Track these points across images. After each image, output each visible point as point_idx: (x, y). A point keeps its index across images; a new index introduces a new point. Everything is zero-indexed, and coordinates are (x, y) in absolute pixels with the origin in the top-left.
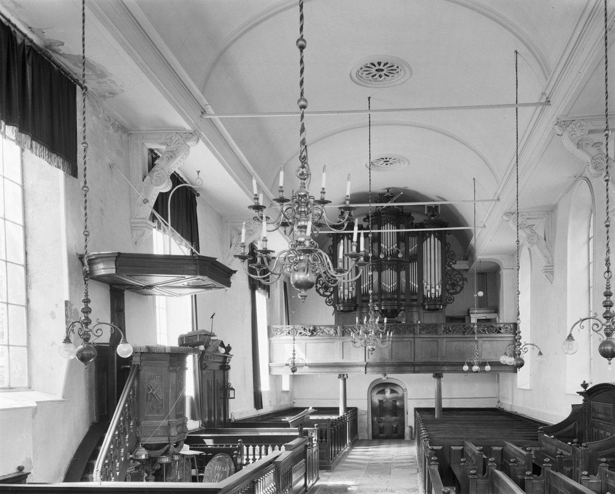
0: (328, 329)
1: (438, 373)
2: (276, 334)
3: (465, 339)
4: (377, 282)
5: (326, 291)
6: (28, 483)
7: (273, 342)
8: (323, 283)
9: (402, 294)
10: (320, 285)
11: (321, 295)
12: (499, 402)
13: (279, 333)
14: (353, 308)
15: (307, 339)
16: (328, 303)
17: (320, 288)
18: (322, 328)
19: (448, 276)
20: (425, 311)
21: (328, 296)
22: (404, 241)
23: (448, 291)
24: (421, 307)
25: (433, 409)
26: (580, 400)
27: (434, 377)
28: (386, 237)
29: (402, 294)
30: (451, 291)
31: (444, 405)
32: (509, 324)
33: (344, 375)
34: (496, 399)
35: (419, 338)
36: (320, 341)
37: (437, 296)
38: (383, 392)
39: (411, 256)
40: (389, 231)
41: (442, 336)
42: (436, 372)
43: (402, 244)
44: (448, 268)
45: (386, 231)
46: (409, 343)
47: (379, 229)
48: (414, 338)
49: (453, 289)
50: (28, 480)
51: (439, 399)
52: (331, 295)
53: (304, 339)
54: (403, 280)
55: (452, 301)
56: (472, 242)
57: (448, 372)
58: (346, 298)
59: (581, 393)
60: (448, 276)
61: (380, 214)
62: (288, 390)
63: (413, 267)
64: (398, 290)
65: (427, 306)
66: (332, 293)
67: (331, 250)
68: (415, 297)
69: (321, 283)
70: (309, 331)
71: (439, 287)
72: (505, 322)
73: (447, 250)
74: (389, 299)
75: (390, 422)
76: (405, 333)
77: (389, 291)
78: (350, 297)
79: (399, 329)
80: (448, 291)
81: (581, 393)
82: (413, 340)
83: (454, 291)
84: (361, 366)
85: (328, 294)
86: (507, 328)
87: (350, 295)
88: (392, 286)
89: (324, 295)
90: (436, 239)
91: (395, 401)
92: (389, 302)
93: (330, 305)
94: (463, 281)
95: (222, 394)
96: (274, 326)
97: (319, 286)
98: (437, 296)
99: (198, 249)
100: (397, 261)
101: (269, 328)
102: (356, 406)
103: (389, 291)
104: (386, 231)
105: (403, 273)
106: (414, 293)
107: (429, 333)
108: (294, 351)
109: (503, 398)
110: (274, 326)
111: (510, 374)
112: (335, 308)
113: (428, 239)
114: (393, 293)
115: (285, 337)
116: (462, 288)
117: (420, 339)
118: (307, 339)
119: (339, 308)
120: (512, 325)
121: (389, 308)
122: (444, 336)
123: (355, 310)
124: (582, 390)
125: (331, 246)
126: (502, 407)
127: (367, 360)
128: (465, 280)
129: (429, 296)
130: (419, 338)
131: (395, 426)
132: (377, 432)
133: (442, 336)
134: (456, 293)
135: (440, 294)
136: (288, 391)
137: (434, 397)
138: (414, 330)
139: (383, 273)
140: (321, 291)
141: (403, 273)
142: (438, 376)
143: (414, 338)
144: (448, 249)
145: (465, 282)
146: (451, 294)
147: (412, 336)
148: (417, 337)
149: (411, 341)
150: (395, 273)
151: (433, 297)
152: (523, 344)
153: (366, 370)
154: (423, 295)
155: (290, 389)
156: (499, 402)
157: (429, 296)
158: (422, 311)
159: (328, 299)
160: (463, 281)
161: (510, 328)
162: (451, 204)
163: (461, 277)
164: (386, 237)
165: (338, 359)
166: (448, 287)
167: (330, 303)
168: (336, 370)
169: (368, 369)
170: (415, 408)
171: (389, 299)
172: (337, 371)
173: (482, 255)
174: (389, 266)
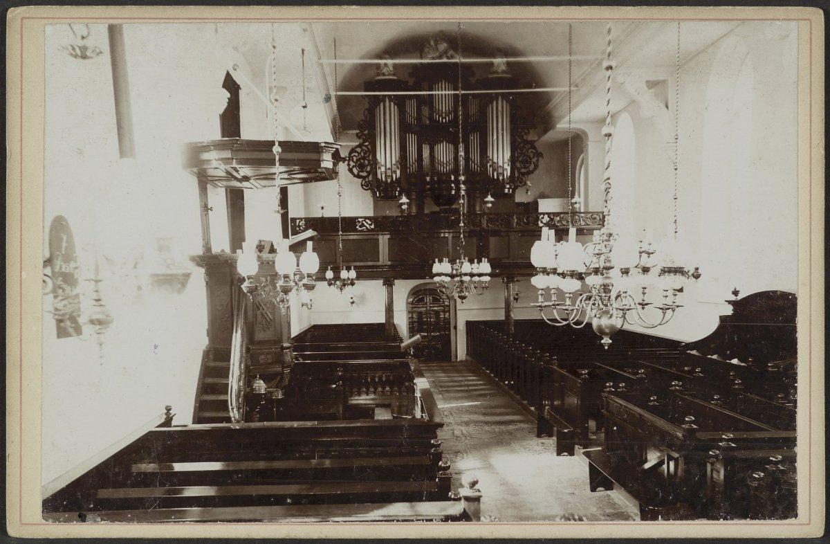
6: (174, 426)
8: (358, 160)
10: (354, 162)
11: (355, 176)
17: (353, 166)
18: (360, 220)
26: (729, 310)
28: (444, 102)
30: (523, 170)
37: (394, 179)
40: (444, 92)
45: (440, 93)
47: (431, 90)
49: (525, 168)
50: (174, 423)
52: (368, 176)
56: (551, 105)
59: (729, 302)
63: (474, 139)
69: (355, 160)
80: (519, 169)
81: (729, 302)
85: (364, 174)
86: (595, 218)
87: (394, 176)
89: (358, 176)
90: (392, 103)
97: (352, 164)
104: (440, 93)
116: (536, 167)
124: (733, 298)
125: (367, 109)
128: (539, 155)
135: (509, 174)
139: (436, 147)
140: (355, 171)
145: (540, 159)
146: (523, 174)
150: (451, 147)
151: (501, 178)
157: (384, 180)
159: (364, 182)
161: (598, 218)
164: (444, 102)
173: (576, 123)
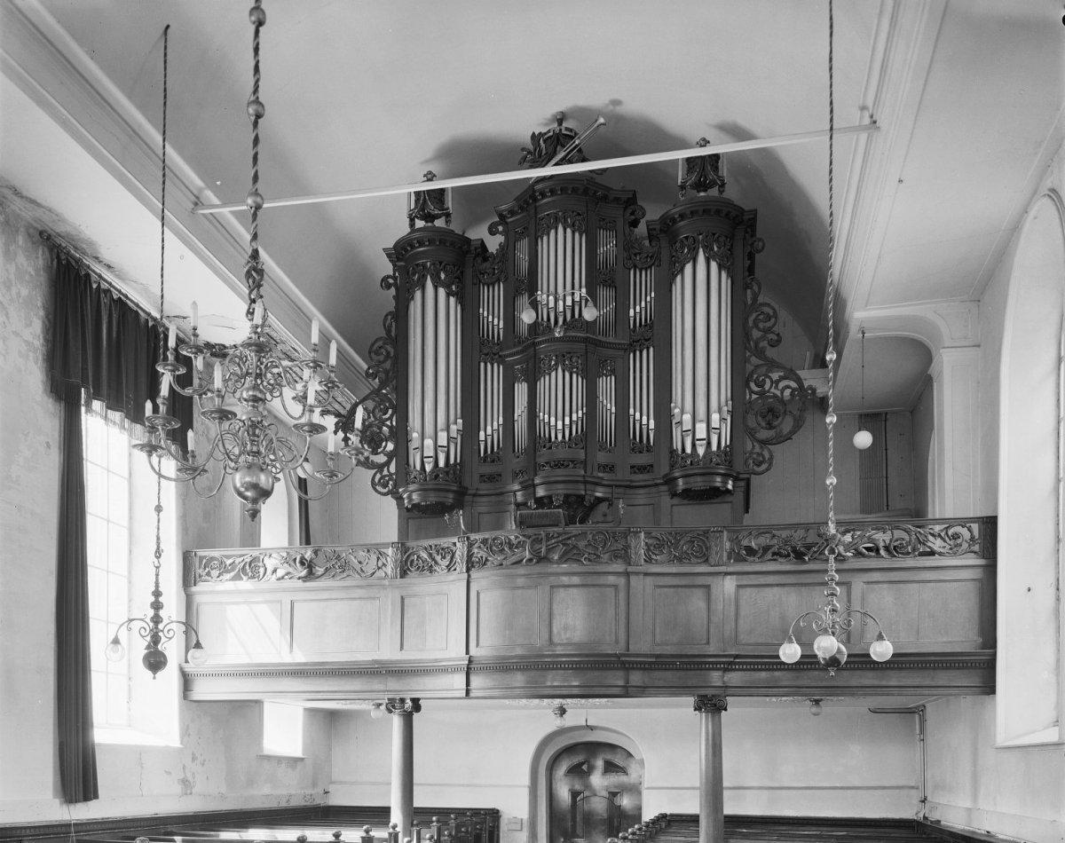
0: (362, 554)
1: (710, 692)
2: (208, 574)
5: (375, 452)
7: (198, 599)
9: (602, 448)
12: (924, 801)
13: (215, 573)
14: (451, 496)
15: (295, 590)
19: (752, 385)
20: (676, 501)
21: (380, 467)
22: (610, 283)
23: (751, 433)
24: (664, 488)
25: (694, 819)
27: (698, 708)
29: (602, 448)
30: (764, 434)
31: (729, 809)
32: (963, 522)
33: (402, 701)
34: (914, 791)
35: (646, 574)
36: (335, 595)
38: (579, 771)
41: (723, 569)
42: (703, 692)
43: (604, 293)
44: (754, 360)
46: (610, 592)
48: (627, 574)
49: (770, 426)
51: (714, 788)
52: (387, 464)
53: (284, 590)
54: (608, 404)
55: (764, 466)
57: (746, 690)
58: (428, 468)
60: (752, 385)
61: (535, 200)
62: (298, 753)
64: (587, 435)
65: (680, 482)
66: (390, 456)
67: (391, 325)
68: (641, 459)
70: (302, 563)
71: (722, 419)
72: (949, 515)
73: (750, 302)
74: (559, 464)
76: (596, 558)
78: (442, 464)
79: (575, 547)
82: (622, 581)
83: (771, 433)
84: (455, 670)
86: (956, 536)
88: (567, 421)
92: (559, 471)
96: (201, 553)
98: (714, 448)
99: (306, 493)
100: (586, 340)
101: (187, 559)
105: (606, 385)
106: (640, 447)
107: (680, 560)
108: (157, 594)
109: (936, 787)
110: (201, 553)
111: (966, 702)
112: (399, 499)
114: (572, 442)
115: (230, 585)
117: (649, 580)
118: (295, 590)
119: (410, 497)
120: (975, 527)
121: (561, 490)
122: (731, 569)
123: (459, 504)
126: (934, 816)
127: (473, 651)
129: (689, 450)
130: (646, 574)
133: (723, 569)
134: (782, 439)
136: (302, 759)
137: (698, 785)
138: (627, 548)
139: (540, 385)
141: (606, 385)
142: (712, 705)
143: (627, 574)
144: (755, 299)
146: (764, 443)
147: (618, 567)
148: (637, 574)
149: (616, 587)
152: (165, 621)
153: (468, 684)
154: (672, 452)
155: (305, 750)
156: (924, 801)
158: (666, 500)
159: (378, 476)
162: (764, 150)
163: (793, 384)
165: (388, 652)
166: (752, 422)
167: (385, 486)
168: (377, 685)
169: (476, 681)
171: (559, 464)
172: (381, 687)
174: (561, 358)
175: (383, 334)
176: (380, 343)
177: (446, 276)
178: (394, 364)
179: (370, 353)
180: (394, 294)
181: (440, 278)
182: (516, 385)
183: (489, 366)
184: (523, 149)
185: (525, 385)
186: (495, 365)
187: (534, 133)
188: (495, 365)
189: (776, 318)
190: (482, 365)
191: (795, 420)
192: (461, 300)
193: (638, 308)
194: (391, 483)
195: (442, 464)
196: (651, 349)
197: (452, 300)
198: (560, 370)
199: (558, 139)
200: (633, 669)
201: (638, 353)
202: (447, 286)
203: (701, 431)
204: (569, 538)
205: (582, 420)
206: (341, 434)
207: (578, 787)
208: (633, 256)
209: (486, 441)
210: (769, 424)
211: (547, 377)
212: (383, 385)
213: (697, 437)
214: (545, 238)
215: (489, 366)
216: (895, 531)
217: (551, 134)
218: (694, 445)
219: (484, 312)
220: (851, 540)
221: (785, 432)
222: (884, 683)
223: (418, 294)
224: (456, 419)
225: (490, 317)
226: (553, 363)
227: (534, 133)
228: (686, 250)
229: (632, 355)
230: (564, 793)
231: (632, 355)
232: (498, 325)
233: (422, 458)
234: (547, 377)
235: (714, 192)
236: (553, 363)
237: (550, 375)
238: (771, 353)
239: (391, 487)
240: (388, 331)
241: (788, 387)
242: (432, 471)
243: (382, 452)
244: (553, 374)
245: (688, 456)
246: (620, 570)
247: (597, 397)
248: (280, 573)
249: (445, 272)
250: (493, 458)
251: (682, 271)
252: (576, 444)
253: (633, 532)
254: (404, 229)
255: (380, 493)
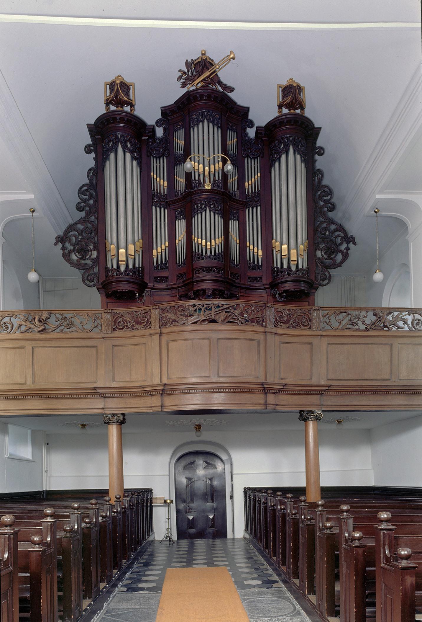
3: (368, 340)
4: (184, 241)
10: (72, 245)
16: (87, 282)
39: (248, 195)
55: (326, 282)
75: (204, 511)
77: (209, 253)
82: (261, 337)
91: (211, 479)
93: (91, 286)
94: (348, 243)
95: (44, 503)
102: (302, 85)
103: (209, 253)
105: (234, 225)
113: (284, 157)
116: (346, 256)
117: (277, 337)
131: (211, 517)
132: (185, 525)
139: (195, 221)
141: (234, 225)
147: (261, 329)
160: (348, 243)
163: (342, 235)
170: (245, 489)
175: (87, 181)
176: (86, 188)
177: (131, 146)
178: (96, 201)
179: (78, 194)
180: (94, 157)
181: (127, 146)
182: (177, 221)
183: (158, 209)
184: (180, 71)
185: (184, 222)
186: (162, 209)
187: (187, 61)
188: (162, 209)
189: (331, 195)
190: (154, 208)
191: (343, 256)
192: (140, 165)
193: (253, 179)
194: (95, 279)
195: (131, 266)
196: (259, 208)
197: (135, 163)
198: (208, 210)
199: (205, 64)
200: (270, 393)
201: (251, 209)
202: (132, 152)
203: (293, 257)
204: (228, 308)
205: (222, 244)
206: (60, 245)
207: (190, 475)
208: (247, 149)
209: (157, 256)
210: (329, 257)
211: (199, 215)
212: (88, 214)
213: (291, 259)
214: (196, 128)
215: (158, 209)
216: (415, 315)
217: (200, 60)
218: (289, 263)
219: (154, 175)
220: (392, 319)
221: (338, 262)
222: (411, 403)
223: (112, 156)
224: (139, 240)
225: (158, 179)
226: (203, 206)
227: (187, 61)
228: (282, 146)
229: (247, 210)
230: (183, 480)
231: (247, 210)
232: (164, 184)
233: (118, 261)
234: (199, 215)
235: (298, 111)
236: (203, 206)
237: (201, 213)
238: (330, 214)
239: (95, 282)
240: (91, 180)
241: (339, 236)
242: (125, 271)
243: (88, 259)
244: (204, 213)
245: (286, 270)
246: (262, 330)
247: (229, 232)
248: (23, 328)
249: (130, 143)
250: (163, 266)
251: (279, 160)
252: (218, 258)
253: (268, 307)
254: (102, 110)
255: (87, 285)
